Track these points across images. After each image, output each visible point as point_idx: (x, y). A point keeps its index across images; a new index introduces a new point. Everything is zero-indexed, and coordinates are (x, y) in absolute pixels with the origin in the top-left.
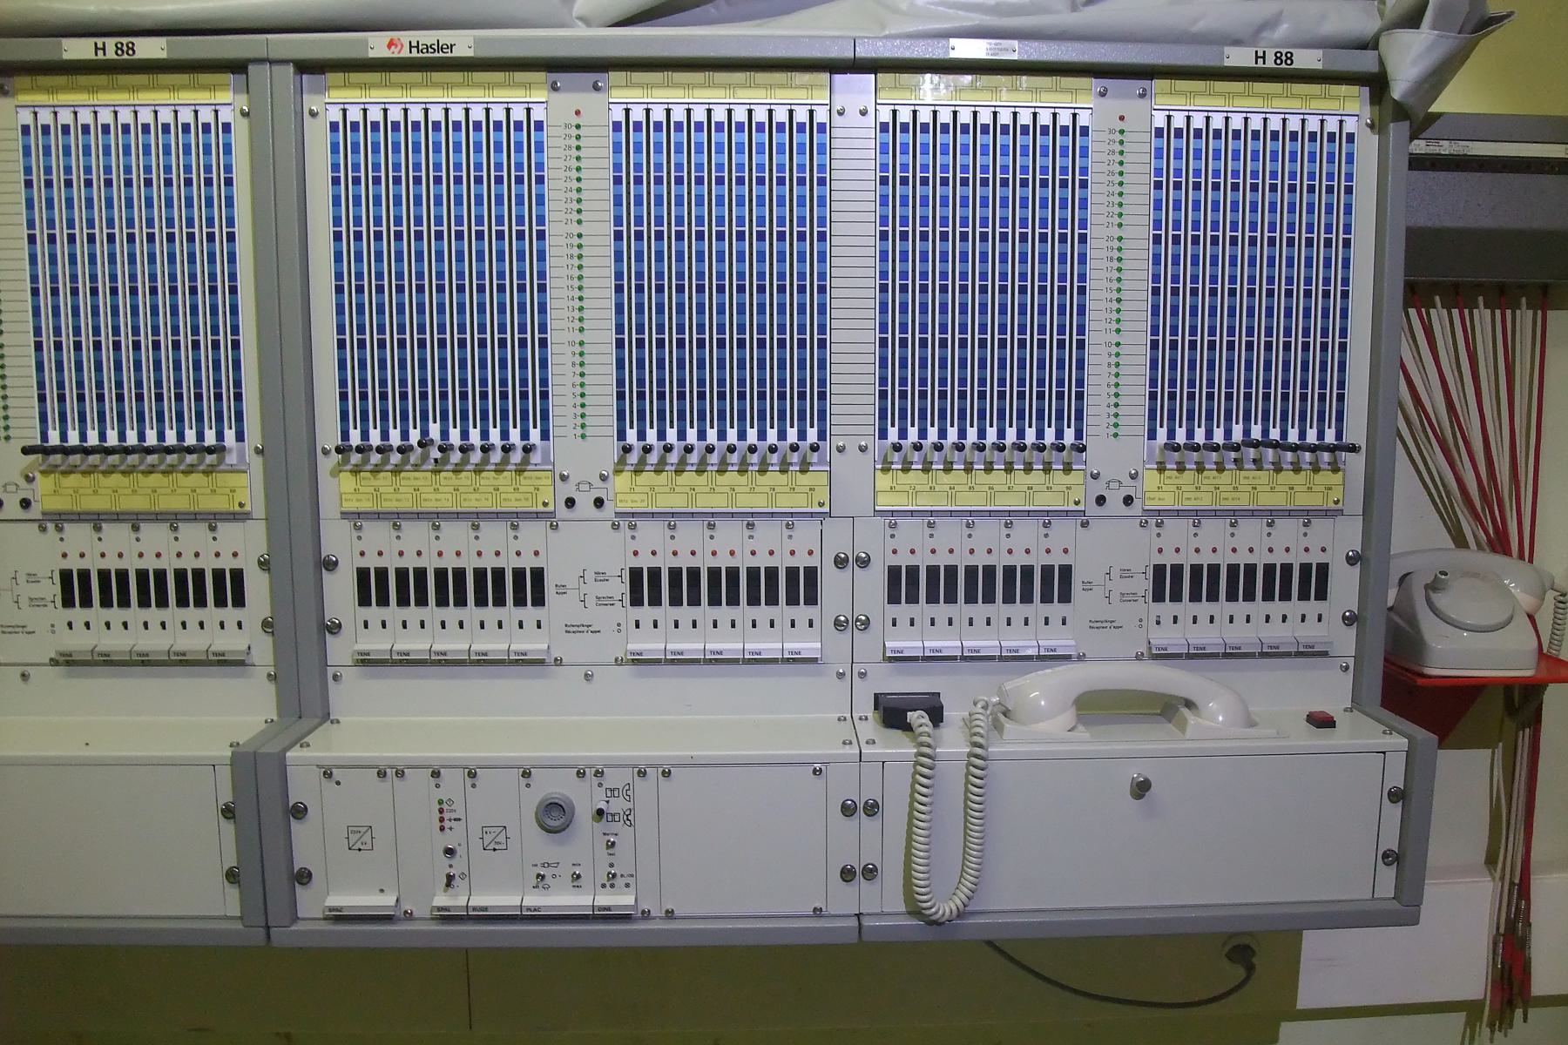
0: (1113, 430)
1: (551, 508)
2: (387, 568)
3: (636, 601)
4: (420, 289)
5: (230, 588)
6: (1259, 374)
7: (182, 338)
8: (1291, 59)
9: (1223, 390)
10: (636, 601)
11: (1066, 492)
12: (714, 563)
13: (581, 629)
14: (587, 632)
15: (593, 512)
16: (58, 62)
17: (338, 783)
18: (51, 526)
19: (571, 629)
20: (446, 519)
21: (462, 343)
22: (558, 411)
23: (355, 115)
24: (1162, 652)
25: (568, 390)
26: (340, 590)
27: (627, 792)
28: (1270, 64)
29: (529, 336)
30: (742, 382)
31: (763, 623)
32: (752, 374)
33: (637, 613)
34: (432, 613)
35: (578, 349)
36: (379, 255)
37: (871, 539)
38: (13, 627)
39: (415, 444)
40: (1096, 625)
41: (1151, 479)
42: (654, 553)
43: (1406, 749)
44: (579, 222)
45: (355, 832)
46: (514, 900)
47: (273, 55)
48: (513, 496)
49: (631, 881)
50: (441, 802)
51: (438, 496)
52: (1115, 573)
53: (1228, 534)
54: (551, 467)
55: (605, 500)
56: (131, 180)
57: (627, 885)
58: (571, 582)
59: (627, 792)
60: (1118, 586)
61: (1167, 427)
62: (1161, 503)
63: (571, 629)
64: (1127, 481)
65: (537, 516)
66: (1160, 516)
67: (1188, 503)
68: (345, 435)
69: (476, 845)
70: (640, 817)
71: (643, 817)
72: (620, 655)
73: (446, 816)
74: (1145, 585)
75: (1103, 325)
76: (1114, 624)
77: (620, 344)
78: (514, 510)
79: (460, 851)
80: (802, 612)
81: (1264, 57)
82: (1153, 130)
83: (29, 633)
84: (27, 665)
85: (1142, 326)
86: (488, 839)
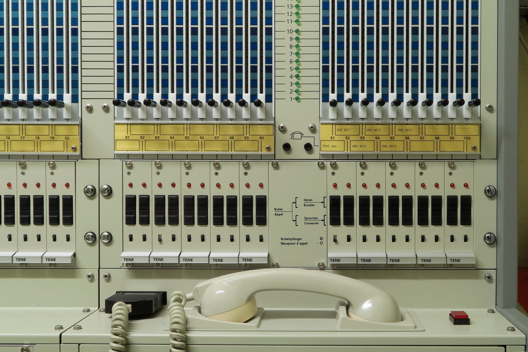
7: (20, 27)
10: (335, 221)
11: (260, 141)
13: (293, 241)
14: (297, 244)
15: (304, 154)
18: (328, 164)
22: (278, 80)
24: (367, 263)
25: (287, 65)
30: (60, 60)
32: (37, 54)
33: (334, 230)
35: (295, 35)
38: (291, 240)
39: (142, 102)
40: (286, 242)
41: (325, 132)
52: (300, 203)
54: (273, 122)
55: (313, 145)
58: (287, 206)
60: (303, 212)
61: (397, 92)
62: (334, 149)
64: (308, 133)
68: (121, 96)
72: (323, 261)
74: (325, 211)
76: (300, 241)
80: (61, 230)
85: (316, 17)
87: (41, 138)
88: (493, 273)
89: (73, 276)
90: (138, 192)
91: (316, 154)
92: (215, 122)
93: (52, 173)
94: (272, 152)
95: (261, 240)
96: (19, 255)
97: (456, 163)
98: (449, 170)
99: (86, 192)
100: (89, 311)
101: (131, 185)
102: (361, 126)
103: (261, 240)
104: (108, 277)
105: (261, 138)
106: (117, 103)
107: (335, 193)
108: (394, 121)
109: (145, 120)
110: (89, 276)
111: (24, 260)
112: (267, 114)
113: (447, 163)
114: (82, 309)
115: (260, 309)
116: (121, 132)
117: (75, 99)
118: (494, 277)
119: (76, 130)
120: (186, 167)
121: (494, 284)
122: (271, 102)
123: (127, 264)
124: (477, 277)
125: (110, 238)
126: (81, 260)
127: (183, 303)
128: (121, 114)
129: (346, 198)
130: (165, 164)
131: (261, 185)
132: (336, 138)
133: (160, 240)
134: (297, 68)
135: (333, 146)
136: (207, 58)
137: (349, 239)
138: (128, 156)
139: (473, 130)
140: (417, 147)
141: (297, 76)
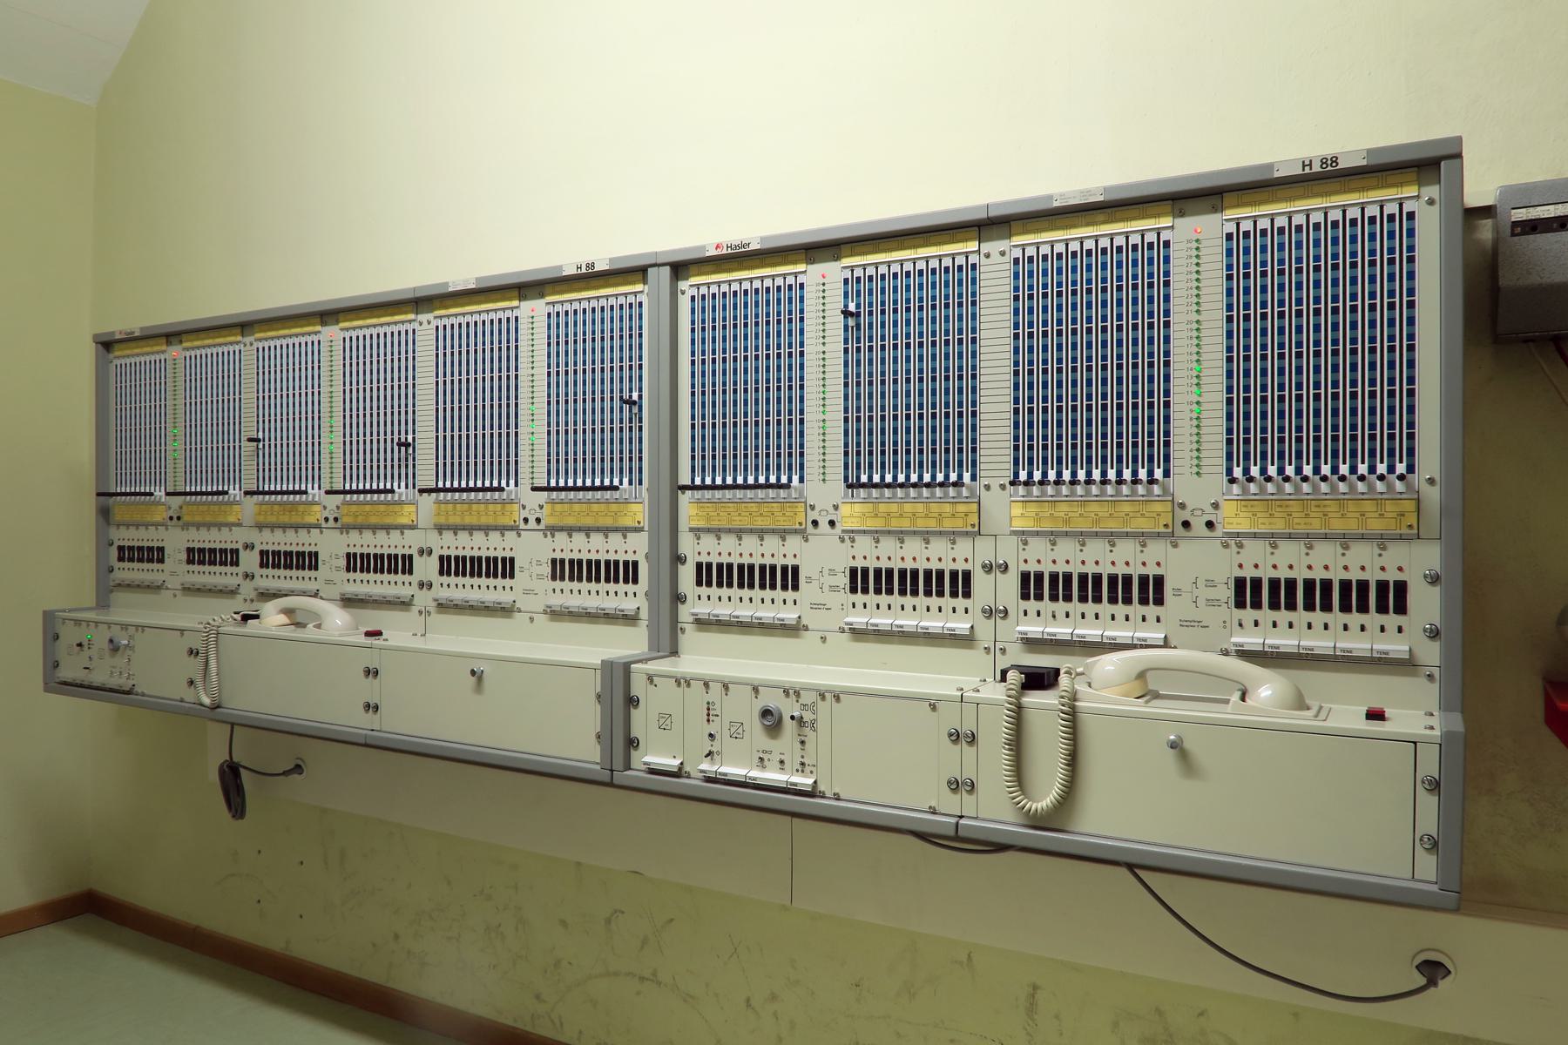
0: (1195, 470)
1: (642, 525)
2: (1072, 573)
3: (1240, 604)
4: (947, 378)
5: (630, 572)
6: (762, 442)
8: (1335, 161)
9: (1109, 441)
12: (1144, 571)
13: (820, 606)
15: (1205, 531)
16: (1271, 179)
17: (656, 686)
18: (847, 538)
19: (816, 606)
20: (407, 529)
21: (947, 415)
23: (1247, 226)
26: (687, 574)
27: (812, 707)
28: (584, 271)
29: (1079, 403)
31: (909, 608)
34: (1301, 616)
36: (947, 356)
37: (1008, 551)
38: (1191, 622)
40: (1186, 624)
41: (1228, 509)
42: (1256, 566)
43: (1439, 742)
44: (824, 344)
45: (663, 717)
46: (742, 772)
47: (659, 261)
48: (782, 519)
49: (813, 769)
50: (708, 703)
51: (740, 518)
53: (696, 544)
54: (1171, 498)
56: (792, 318)
57: (812, 772)
58: (815, 576)
59: (812, 707)
60: (1204, 593)
61: (1369, 463)
63: (816, 606)
64: (831, 510)
65: (796, 532)
66: (851, 535)
67: (1263, 527)
68: (1016, 475)
69: (726, 733)
70: (820, 725)
71: (822, 725)
72: (1225, 646)
73: (711, 712)
74: (845, 580)
75: (815, 409)
76: (1201, 624)
77: (1229, 401)
78: (716, 526)
79: (718, 737)
80: (960, 602)
81: (1310, 165)
82: (1224, 235)
83: (827, 609)
84: (532, 612)
86: (733, 730)
87: (917, 515)
88: (1436, 672)
89: (971, 647)
90: (1032, 568)
91: (1219, 531)
92: (1050, 499)
93: (952, 548)
94: (1170, 530)
95: (1158, 620)
96: (922, 624)
97: (1350, 544)
98: (1270, 550)
99: (984, 566)
100: (985, 680)
101: (1026, 561)
102: (1379, 501)
103: (1158, 620)
104: (1003, 651)
105: (1158, 515)
106: (1012, 483)
107: (1240, 574)
108: (1384, 496)
109: (1041, 496)
110: (986, 648)
111: (927, 629)
112: (1165, 490)
113: (1302, 543)
114: (979, 679)
115: (1151, 687)
116: (1017, 510)
117: (974, 478)
118: (1437, 676)
119: (975, 506)
120: (1307, 547)
121: (1437, 685)
122: (1414, 473)
123: (1022, 639)
124: (1414, 674)
125: (1006, 612)
126: (979, 633)
127: (1073, 676)
128: (1016, 493)
129: (596, 561)
130: (1281, 543)
131: (1158, 564)
132: (1242, 515)
133: (1054, 616)
134: (1198, 442)
135: (1237, 524)
136: (1148, 432)
137: (1256, 624)
138: (1023, 533)
139: (1410, 506)
140: (1337, 526)
141: (1198, 450)
